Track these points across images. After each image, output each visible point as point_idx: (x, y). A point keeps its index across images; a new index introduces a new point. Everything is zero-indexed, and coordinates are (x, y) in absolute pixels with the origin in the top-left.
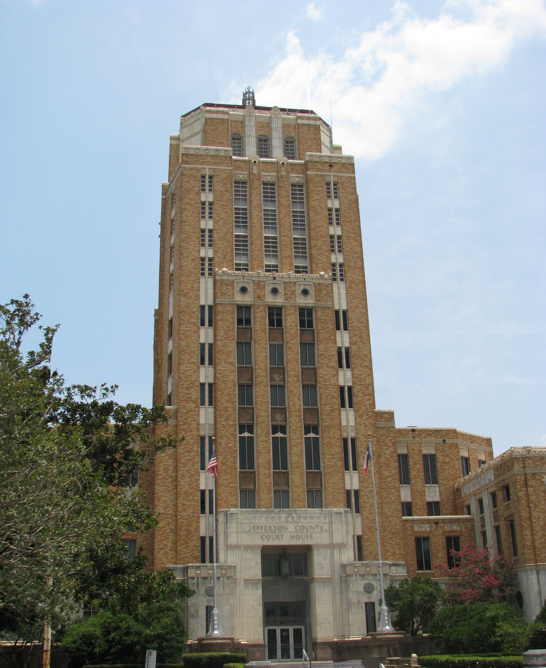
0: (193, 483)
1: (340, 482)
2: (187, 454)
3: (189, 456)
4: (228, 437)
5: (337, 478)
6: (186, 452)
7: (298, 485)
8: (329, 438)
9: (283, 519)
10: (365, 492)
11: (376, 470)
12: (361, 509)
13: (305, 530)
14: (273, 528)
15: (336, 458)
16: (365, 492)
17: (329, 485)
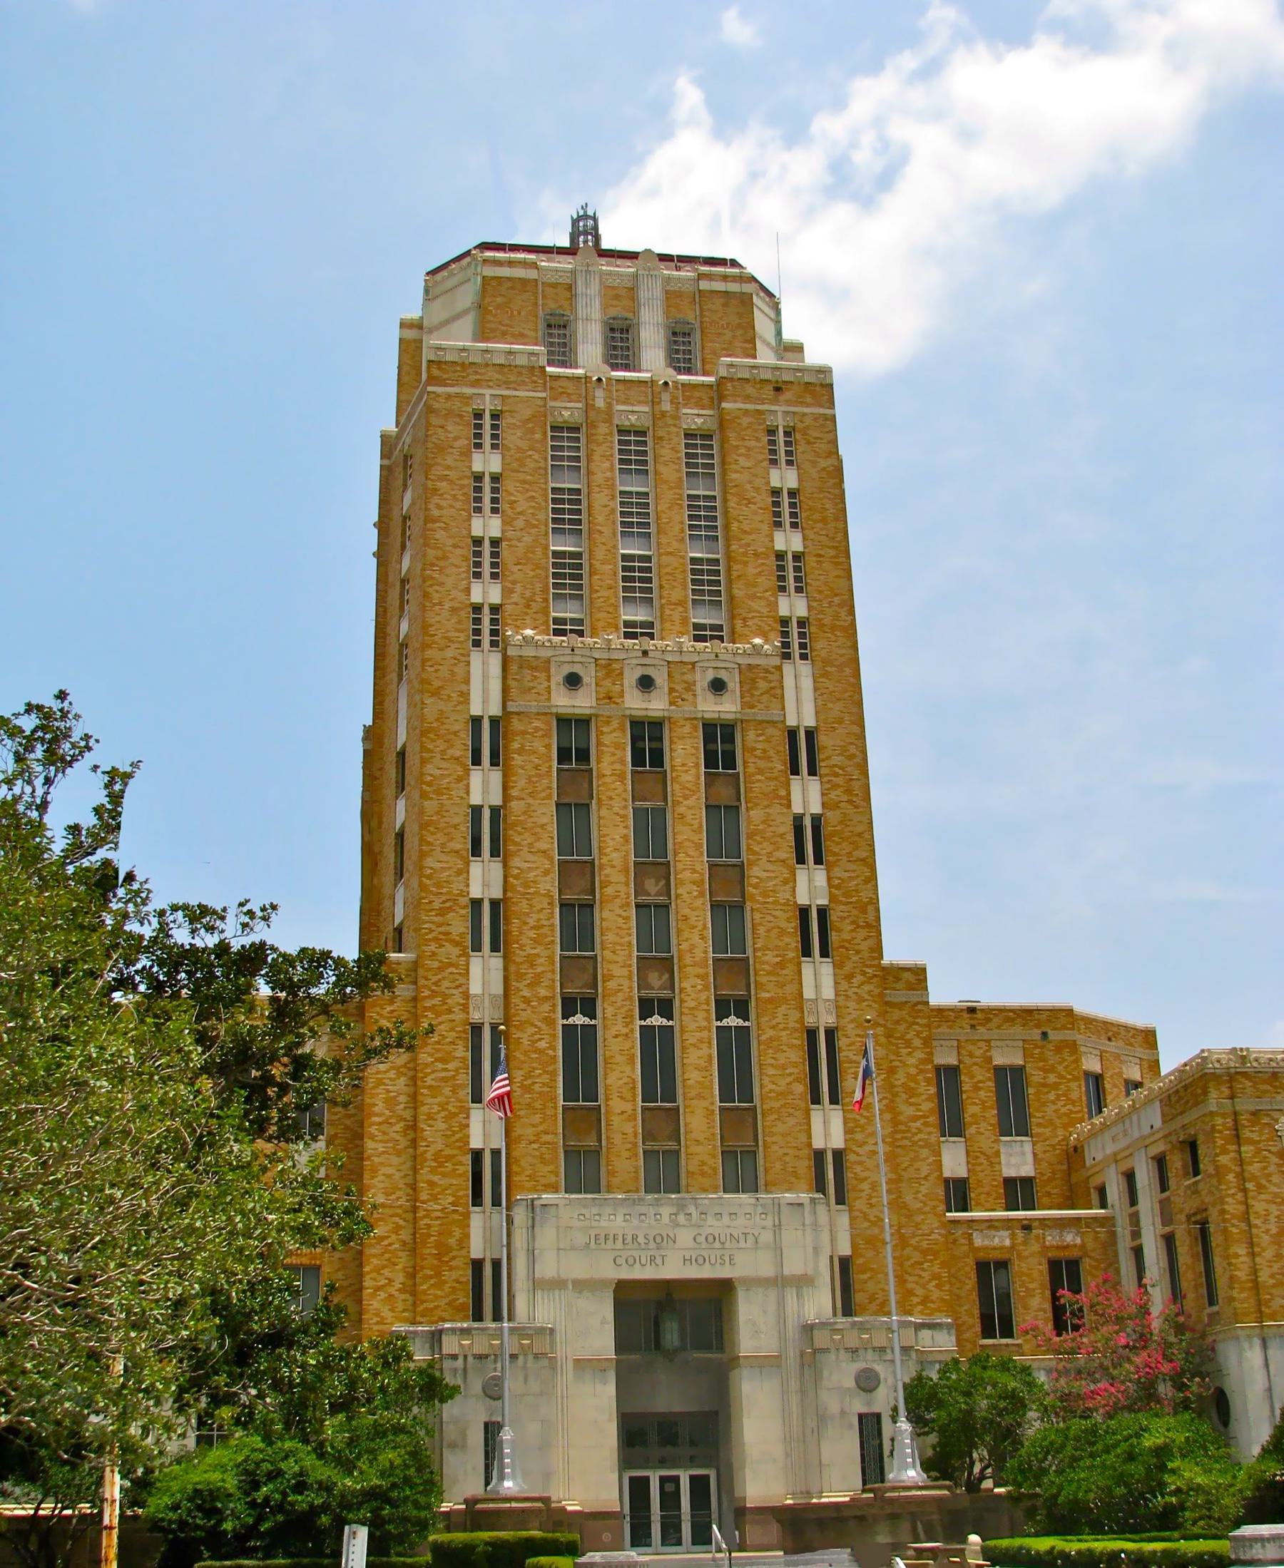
0: (454, 1133)
1: (800, 1131)
2: (440, 1066)
3: (446, 1070)
4: (536, 1026)
5: (792, 1121)
6: (437, 1060)
7: (701, 1138)
8: (773, 1027)
9: (666, 1219)
10: (858, 1154)
11: (884, 1102)
12: (850, 1196)
13: (717, 1245)
14: (641, 1239)
15: (790, 1074)
16: (858, 1154)
17: (774, 1139)
